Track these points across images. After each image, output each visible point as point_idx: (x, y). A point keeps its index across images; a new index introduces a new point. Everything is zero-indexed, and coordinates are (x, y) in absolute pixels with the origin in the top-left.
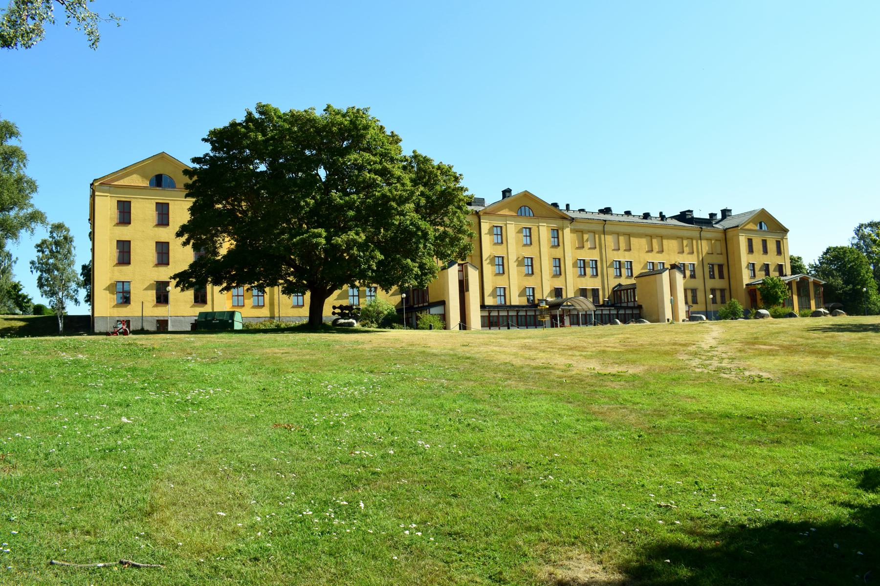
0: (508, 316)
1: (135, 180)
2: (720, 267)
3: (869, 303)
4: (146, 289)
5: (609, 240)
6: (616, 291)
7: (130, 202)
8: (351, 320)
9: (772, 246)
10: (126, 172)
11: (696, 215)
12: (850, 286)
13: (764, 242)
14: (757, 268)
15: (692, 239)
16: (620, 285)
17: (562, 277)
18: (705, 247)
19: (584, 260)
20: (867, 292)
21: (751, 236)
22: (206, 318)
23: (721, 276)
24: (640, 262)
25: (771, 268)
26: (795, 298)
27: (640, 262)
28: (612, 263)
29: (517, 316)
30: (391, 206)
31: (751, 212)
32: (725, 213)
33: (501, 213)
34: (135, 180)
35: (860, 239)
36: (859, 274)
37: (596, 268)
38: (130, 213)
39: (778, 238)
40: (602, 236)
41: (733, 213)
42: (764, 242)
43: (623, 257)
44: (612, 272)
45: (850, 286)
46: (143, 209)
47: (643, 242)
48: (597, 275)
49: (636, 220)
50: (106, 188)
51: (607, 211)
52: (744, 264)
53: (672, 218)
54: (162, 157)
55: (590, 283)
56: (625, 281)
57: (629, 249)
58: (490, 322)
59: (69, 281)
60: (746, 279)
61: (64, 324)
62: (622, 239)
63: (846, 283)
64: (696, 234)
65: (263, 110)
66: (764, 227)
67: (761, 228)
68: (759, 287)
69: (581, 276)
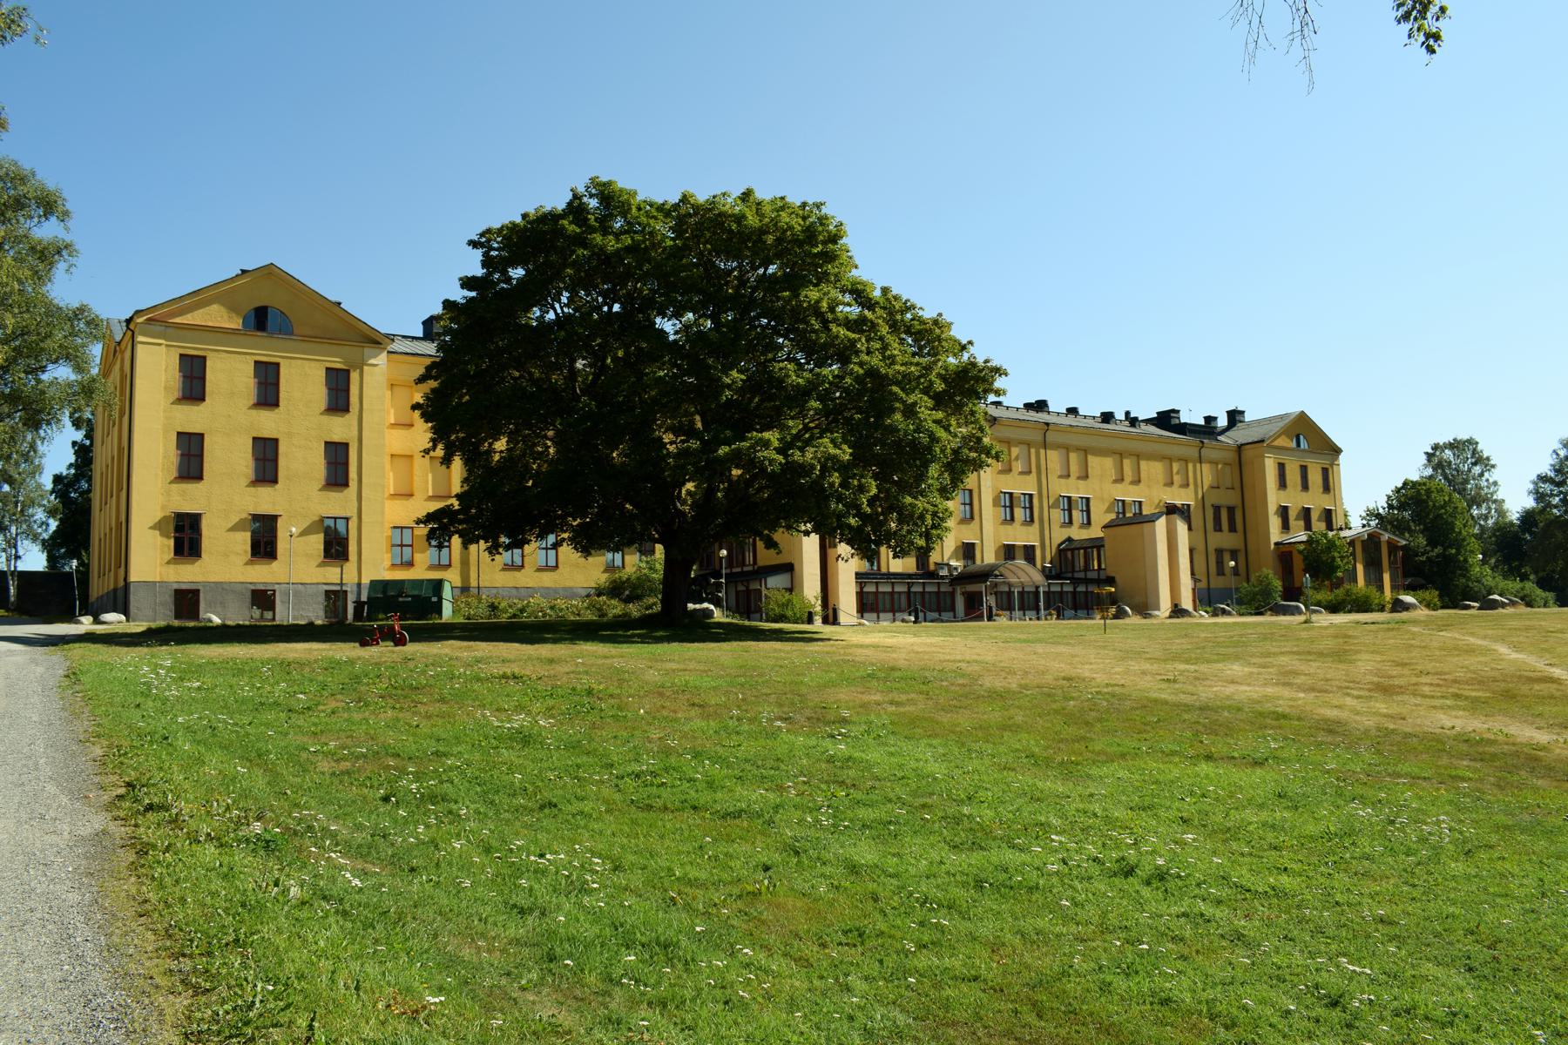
0: (892, 593)
1: (215, 316)
2: (1231, 510)
3: (1469, 579)
4: (233, 529)
5: (1054, 458)
6: (1065, 550)
7: (204, 358)
8: (705, 605)
9: (1315, 477)
10: (198, 298)
11: (1185, 418)
12: (1438, 550)
13: (1304, 469)
14: (1292, 514)
15: (1186, 461)
16: (1069, 539)
17: (975, 524)
18: (1207, 475)
19: (1011, 494)
20: (1466, 560)
21: (193, 349)
22: (384, 592)
23: (1233, 529)
24: (1102, 499)
25: (1314, 516)
26: (1360, 568)
27: (1102, 499)
28: (1057, 500)
29: (909, 593)
30: (891, 393)
31: (1281, 417)
32: (1234, 416)
33: (178, 320)
34: (215, 316)
35: (1434, 469)
36: (1453, 529)
37: (1031, 508)
38: (203, 379)
39: (1325, 462)
40: (1042, 451)
41: (1248, 417)
42: (1304, 469)
43: (1077, 490)
44: (1058, 516)
45: (1438, 550)
46: (231, 373)
47: (1108, 463)
48: (1032, 520)
49: (1090, 423)
50: (157, 328)
51: (1041, 406)
52: (1272, 508)
53: (1147, 421)
54: (270, 272)
55: (1022, 536)
56: (1078, 534)
57: (1085, 476)
58: (866, 605)
59: (33, 503)
60: (1275, 535)
61: (19, 588)
62: (1073, 457)
63: (1432, 543)
64: (1193, 452)
65: (607, 194)
66: (1304, 444)
67: (1298, 444)
68: (1302, 547)
69: (1005, 522)
